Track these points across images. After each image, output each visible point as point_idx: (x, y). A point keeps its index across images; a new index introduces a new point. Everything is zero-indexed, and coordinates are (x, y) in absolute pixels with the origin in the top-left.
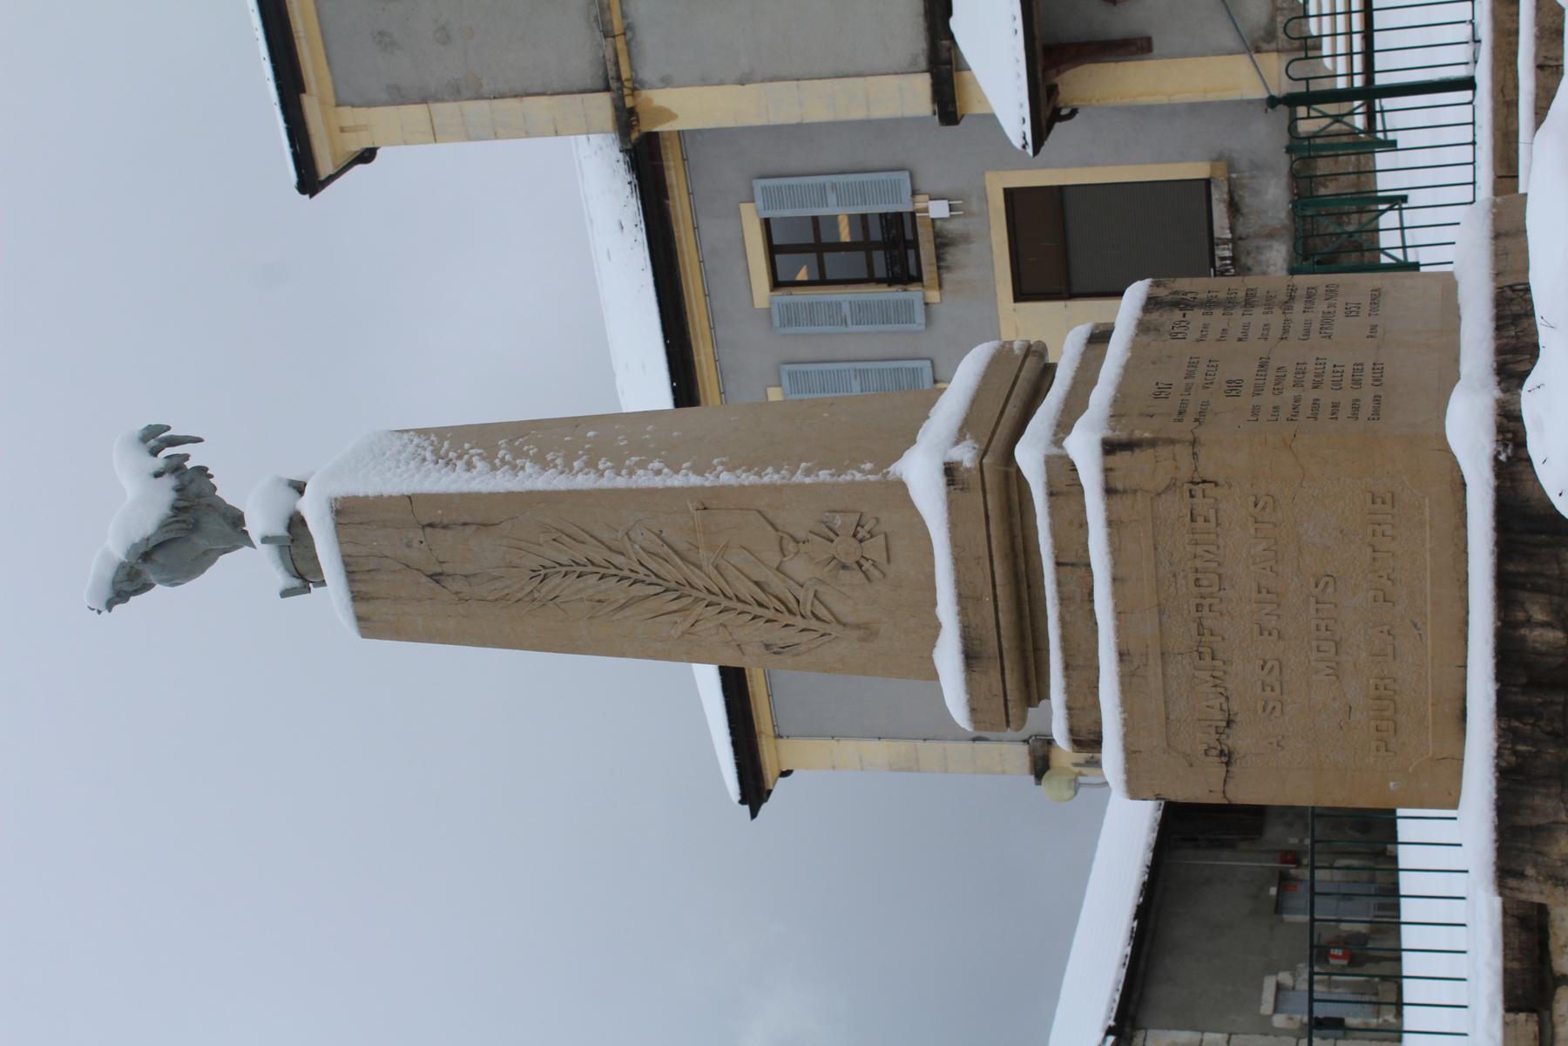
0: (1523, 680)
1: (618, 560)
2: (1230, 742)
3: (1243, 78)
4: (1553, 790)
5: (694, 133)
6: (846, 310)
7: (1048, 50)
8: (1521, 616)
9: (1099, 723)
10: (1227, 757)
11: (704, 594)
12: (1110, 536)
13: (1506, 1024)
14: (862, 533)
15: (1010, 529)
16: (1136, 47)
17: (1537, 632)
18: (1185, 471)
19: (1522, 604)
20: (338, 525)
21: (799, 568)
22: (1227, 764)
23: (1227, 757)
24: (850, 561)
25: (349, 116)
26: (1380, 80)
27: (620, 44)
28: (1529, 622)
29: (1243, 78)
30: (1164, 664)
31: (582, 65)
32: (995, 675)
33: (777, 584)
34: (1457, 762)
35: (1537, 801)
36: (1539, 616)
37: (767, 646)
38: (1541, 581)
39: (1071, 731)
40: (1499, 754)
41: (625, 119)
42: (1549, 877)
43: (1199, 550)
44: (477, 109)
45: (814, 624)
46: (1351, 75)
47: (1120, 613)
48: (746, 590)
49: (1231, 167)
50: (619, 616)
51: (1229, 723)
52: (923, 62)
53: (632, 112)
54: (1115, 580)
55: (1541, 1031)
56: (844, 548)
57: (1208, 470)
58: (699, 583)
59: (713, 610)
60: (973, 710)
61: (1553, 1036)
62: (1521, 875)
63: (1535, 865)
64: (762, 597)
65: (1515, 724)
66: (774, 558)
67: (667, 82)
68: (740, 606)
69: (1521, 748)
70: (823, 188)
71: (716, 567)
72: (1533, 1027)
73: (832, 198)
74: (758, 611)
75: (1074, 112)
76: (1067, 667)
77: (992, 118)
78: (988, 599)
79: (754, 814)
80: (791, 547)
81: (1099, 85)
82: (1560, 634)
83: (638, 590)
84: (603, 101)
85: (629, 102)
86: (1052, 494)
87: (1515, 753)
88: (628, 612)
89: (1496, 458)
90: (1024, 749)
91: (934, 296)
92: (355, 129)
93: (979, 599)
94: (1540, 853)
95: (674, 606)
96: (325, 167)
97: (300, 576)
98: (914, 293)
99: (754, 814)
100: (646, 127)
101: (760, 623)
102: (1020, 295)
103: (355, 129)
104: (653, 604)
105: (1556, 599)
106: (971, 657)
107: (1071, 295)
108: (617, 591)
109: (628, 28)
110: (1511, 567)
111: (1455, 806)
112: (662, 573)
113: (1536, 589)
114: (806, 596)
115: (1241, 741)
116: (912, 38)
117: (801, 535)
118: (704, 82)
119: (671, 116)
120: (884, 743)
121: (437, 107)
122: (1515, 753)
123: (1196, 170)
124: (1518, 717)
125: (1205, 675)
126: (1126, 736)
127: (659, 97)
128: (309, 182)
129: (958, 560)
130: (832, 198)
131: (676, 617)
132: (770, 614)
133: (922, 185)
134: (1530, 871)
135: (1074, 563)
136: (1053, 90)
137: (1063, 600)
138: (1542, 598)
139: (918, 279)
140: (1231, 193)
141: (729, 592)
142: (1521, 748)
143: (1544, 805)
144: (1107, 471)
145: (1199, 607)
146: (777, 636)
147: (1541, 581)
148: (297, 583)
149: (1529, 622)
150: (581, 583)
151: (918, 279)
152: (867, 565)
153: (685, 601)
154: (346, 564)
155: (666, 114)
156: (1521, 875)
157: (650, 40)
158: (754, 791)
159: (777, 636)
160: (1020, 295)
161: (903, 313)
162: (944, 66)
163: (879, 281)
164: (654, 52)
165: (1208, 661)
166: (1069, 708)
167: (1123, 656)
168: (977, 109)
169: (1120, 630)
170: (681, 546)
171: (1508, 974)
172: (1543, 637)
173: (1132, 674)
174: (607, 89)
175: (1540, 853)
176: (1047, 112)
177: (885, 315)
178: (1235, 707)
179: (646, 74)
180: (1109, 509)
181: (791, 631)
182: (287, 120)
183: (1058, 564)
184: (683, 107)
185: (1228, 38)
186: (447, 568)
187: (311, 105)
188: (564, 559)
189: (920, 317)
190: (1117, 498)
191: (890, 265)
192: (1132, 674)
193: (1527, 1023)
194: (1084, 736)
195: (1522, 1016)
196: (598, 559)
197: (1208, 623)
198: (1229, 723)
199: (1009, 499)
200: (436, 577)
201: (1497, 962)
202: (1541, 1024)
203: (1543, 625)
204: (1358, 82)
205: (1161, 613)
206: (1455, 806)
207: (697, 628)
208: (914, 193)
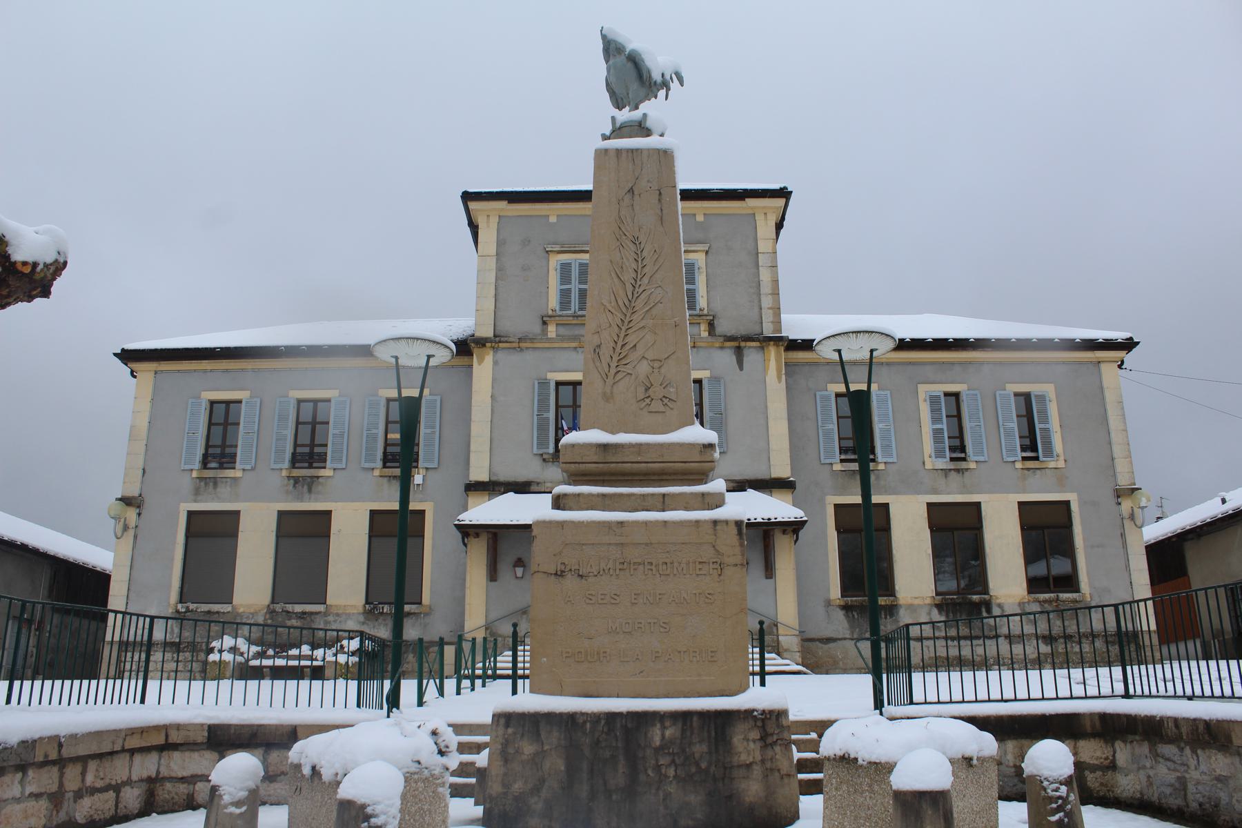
0: (629, 725)
1: (646, 280)
2: (569, 576)
3: (474, 622)
4: (563, 742)
5: (470, 375)
6: (374, 431)
7: (495, 535)
8: (667, 724)
9: (570, 509)
10: (560, 574)
11: (628, 319)
12: (690, 521)
13: (202, 725)
14: (666, 401)
15: (675, 473)
16: (493, 575)
17: (659, 732)
18: (727, 560)
19: (674, 724)
20: (658, 150)
21: (644, 368)
22: (556, 574)
23: (560, 574)
24: (651, 392)
25: (494, 221)
26: (767, 669)
27: (516, 345)
28: (664, 728)
29: (474, 622)
30: (617, 544)
31: (507, 326)
32: (595, 459)
33: (634, 357)
34: (561, 693)
35: (555, 734)
36: (668, 733)
37: (599, 346)
38: (688, 733)
39: (565, 495)
40: (582, 714)
41: (482, 342)
42: (507, 740)
43: (684, 565)
44: (492, 277)
45: (613, 371)
46: (524, 669)
47: (646, 523)
48: (632, 339)
49: (426, 614)
50: (614, 275)
51: (581, 576)
52: (494, 478)
53: (484, 345)
54: (665, 522)
55: (195, 744)
56: (657, 392)
57: (728, 571)
58: (635, 317)
59: (619, 323)
60: (573, 446)
61: (193, 750)
62: (507, 725)
63: (515, 733)
64: (627, 347)
65: (603, 722)
66: (650, 355)
67: (495, 363)
68: (622, 336)
69: (588, 725)
70: (434, 427)
71: (644, 327)
72: (200, 739)
73: (429, 431)
74: (620, 344)
75: (465, 545)
76: (604, 495)
77: (466, 509)
78: (639, 459)
79: (115, 354)
80: (656, 365)
81: (478, 554)
82: (658, 743)
83: (629, 288)
84: (490, 334)
85: (488, 345)
86: (703, 494)
87: (585, 722)
88: (616, 280)
89: (754, 710)
90: (136, 494)
91: (377, 473)
92: (488, 222)
93: (639, 455)
94: (523, 735)
95: (621, 303)
96: (473, 205)
97: (620, 128)
98: (379, 464)
99: (115, 354)
100: (476, 352)
101: (612, 344)
102: (373, 513)
103: (488, 222)
104: (621, 293)
105: (678, 741)
106: (605, 447)
107: (370, 537)
108: (628, 276)
109: (521, 350)
110: (695, 719)
111: (531, 692)
112: (639, 300)
113: (683, 731)
114: (628, 369)
115: (570, 582)
116: (504, 475)
117: (663, 370)
118: (494, 380)
119: (480, 362)
120: (146, 424)
121: (494, 259)
122: (585, 722)
123: (426, 599)
124: (607, 723)
125: (610, 565)
126: (572, 522)
127: (489, 358)
128: (467, 197)
129: (661, 446)
130: (429, 431)
131: (614, 303)
132: (618, 350)
133: (430, 473)
134: (510, 731)
135: (664, 503)
136: (477, 535)
137: (643, 496)
138: (678, 734)
139: (384, 467)
140: (414, 613)
141: (630, 331)
142: (588, 725)
143: (553, 738)
144: (727, 522)
145: (651, 564)
146: (605, 352)
147: (688, 733)
148: (618, 125)
149: (664, 728)
150: (631, 260)
151: (384, 467)
152: (648, 401)
153: (624, 310)
154: (637, 150)
155: (481, 361)
156: (507, 725)
157: (515, 358)
158: (127, 356)
159: (605, 352)
160: (373, 513)
161: (370, 457)
162: (492, 488)
163: (385, 449)
164: (510, 359)
165: (619, 566)
166: (579, 495)
167: (621, 524)
168: (471, 500)
169: (636, 523)
170: (654, 311)
171: (229, 726)
172: (655, 735)
173: (610, 528)
174: (495, 336)
175: (523, 735)
176: (467, 531)
177: (280, 452)
178: (590, 580)
179: (500, 355)
180: (705, 521)
181: (609, 359)
182: (497, 193)
183: (664, 495)
184: (484, 368)
185: (493, 616)
186: (636, 197)
187: (502, 205)
188: (645, 253)
189: (367, 465)
190: (711, 525)
191: (393, 454)
192: (610, 528)
193: (202, 737)
194: (562, 502)
195: (206, 734)
196: (646, 270)
197: (641, 567)
198: (581, 576)
199: (691, 474)
200: (631, 191)
201: (234, 721)
202: (202, 743)
203: (663, 735)
204: (520, 672)
205: (647, 544)
206: (531, 692)
207: (609, 315)
208: (427, 469)
